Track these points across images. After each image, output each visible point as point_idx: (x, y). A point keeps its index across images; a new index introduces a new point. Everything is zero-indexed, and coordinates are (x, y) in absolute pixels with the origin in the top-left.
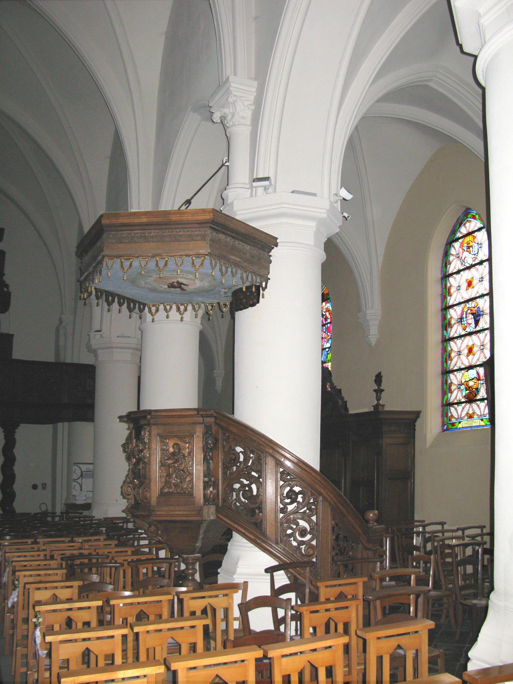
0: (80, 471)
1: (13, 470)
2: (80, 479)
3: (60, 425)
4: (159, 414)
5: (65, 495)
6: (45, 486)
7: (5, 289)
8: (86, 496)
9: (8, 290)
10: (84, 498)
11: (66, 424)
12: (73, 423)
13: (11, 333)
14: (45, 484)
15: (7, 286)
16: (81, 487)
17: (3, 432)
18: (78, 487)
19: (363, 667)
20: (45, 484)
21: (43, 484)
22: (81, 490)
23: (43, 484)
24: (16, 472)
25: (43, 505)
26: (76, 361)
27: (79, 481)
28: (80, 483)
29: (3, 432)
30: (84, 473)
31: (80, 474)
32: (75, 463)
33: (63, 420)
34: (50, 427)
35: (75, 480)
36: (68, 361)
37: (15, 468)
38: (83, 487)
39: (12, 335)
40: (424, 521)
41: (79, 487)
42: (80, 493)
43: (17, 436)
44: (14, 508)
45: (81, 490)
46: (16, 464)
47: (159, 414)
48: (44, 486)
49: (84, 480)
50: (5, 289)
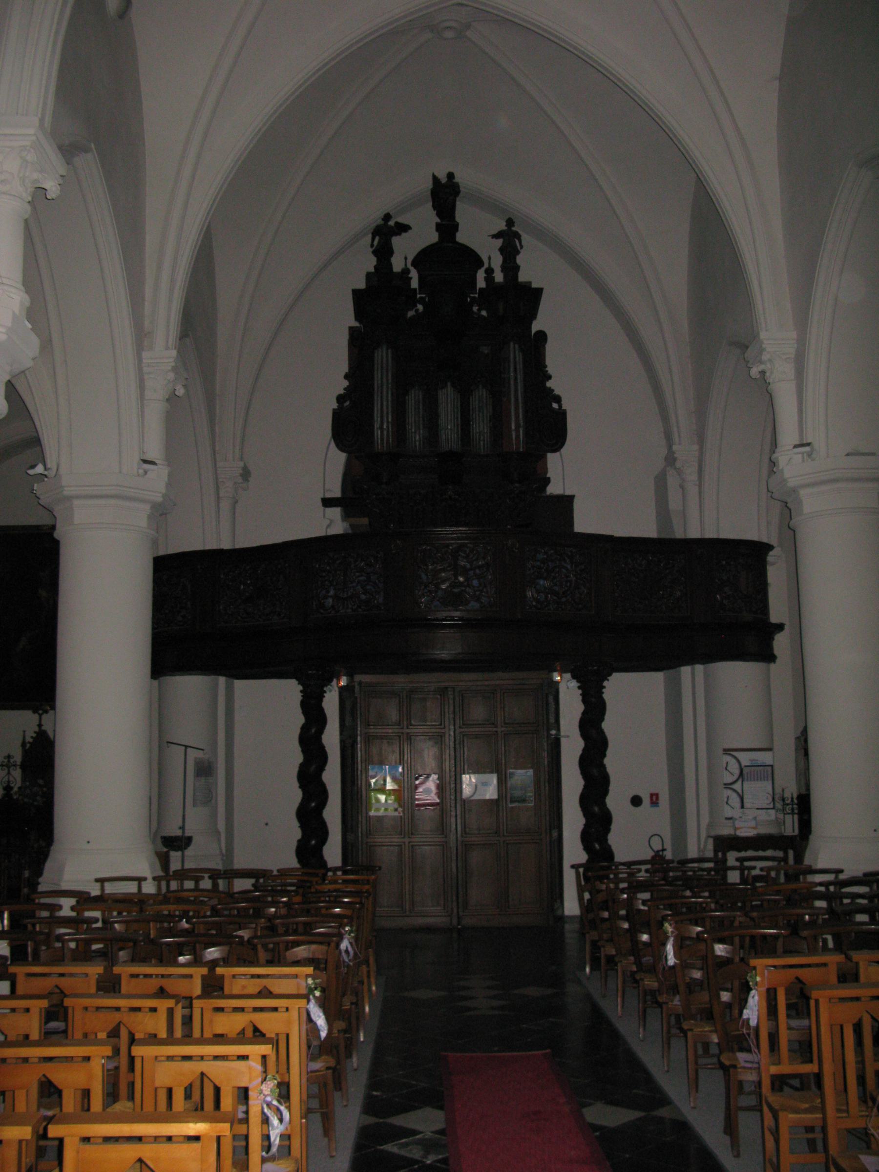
0: (737, 766)
1: (604, 767)
2: (740, 782)
3: (686, 671)
4: (551, 699)
5: (705, 820)
6: (657, 798)
7: (555, 406)
8: (755, 818)
9: (560, 406)
10: (753, 824)
11: (699, 668)
12: (712, 665)
13: (568, 493)
14: (657, 795)
15: (558, 399)
16: (742, 799)
17: (579, 688)
18: (735, 800)
19: (820, 1116)
20: (657, 795)
21: (652, 795)
22: (742, 807)
23: (652, 795)
24: (610, 769)
25: (656, 838)
26: (710, 534)
27: (737, 786)
28: (740, 791)
29: (579, 688)
30: (745, 771)
31: (737, 772)
32: (725, 750)
33: (692, 660)
34: (657, 678)
35: (728, 786)
36: (694, 533)
37: (607, 761)
38: (745, 801)
39: (571, 499)
40: (841, 871)
41: (738, 800)
42: (743, 813)
43: (607, 695)
44: (610, 846)
45: (742, 807)
46: (609, 752)
47: (551, 699)
48: (655, 799)
49: (746, 785)
50: (555, 406)
